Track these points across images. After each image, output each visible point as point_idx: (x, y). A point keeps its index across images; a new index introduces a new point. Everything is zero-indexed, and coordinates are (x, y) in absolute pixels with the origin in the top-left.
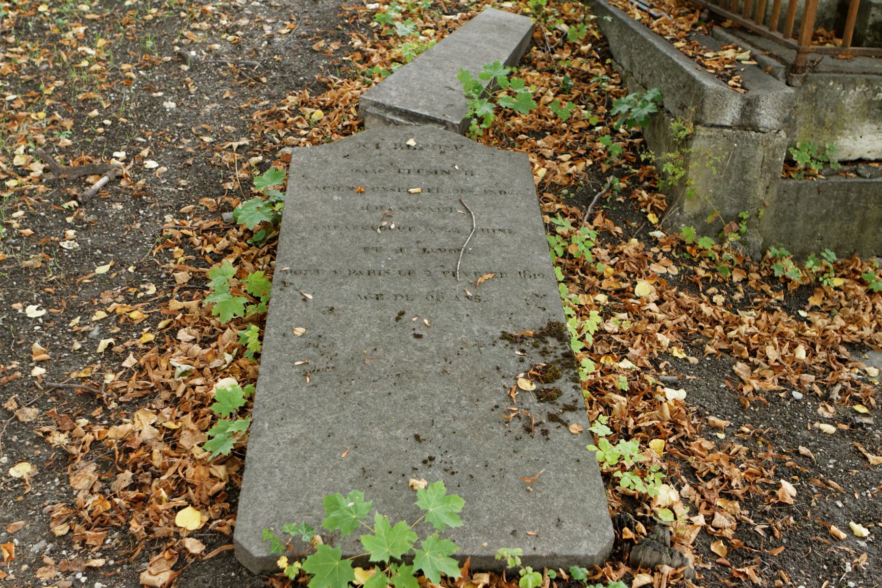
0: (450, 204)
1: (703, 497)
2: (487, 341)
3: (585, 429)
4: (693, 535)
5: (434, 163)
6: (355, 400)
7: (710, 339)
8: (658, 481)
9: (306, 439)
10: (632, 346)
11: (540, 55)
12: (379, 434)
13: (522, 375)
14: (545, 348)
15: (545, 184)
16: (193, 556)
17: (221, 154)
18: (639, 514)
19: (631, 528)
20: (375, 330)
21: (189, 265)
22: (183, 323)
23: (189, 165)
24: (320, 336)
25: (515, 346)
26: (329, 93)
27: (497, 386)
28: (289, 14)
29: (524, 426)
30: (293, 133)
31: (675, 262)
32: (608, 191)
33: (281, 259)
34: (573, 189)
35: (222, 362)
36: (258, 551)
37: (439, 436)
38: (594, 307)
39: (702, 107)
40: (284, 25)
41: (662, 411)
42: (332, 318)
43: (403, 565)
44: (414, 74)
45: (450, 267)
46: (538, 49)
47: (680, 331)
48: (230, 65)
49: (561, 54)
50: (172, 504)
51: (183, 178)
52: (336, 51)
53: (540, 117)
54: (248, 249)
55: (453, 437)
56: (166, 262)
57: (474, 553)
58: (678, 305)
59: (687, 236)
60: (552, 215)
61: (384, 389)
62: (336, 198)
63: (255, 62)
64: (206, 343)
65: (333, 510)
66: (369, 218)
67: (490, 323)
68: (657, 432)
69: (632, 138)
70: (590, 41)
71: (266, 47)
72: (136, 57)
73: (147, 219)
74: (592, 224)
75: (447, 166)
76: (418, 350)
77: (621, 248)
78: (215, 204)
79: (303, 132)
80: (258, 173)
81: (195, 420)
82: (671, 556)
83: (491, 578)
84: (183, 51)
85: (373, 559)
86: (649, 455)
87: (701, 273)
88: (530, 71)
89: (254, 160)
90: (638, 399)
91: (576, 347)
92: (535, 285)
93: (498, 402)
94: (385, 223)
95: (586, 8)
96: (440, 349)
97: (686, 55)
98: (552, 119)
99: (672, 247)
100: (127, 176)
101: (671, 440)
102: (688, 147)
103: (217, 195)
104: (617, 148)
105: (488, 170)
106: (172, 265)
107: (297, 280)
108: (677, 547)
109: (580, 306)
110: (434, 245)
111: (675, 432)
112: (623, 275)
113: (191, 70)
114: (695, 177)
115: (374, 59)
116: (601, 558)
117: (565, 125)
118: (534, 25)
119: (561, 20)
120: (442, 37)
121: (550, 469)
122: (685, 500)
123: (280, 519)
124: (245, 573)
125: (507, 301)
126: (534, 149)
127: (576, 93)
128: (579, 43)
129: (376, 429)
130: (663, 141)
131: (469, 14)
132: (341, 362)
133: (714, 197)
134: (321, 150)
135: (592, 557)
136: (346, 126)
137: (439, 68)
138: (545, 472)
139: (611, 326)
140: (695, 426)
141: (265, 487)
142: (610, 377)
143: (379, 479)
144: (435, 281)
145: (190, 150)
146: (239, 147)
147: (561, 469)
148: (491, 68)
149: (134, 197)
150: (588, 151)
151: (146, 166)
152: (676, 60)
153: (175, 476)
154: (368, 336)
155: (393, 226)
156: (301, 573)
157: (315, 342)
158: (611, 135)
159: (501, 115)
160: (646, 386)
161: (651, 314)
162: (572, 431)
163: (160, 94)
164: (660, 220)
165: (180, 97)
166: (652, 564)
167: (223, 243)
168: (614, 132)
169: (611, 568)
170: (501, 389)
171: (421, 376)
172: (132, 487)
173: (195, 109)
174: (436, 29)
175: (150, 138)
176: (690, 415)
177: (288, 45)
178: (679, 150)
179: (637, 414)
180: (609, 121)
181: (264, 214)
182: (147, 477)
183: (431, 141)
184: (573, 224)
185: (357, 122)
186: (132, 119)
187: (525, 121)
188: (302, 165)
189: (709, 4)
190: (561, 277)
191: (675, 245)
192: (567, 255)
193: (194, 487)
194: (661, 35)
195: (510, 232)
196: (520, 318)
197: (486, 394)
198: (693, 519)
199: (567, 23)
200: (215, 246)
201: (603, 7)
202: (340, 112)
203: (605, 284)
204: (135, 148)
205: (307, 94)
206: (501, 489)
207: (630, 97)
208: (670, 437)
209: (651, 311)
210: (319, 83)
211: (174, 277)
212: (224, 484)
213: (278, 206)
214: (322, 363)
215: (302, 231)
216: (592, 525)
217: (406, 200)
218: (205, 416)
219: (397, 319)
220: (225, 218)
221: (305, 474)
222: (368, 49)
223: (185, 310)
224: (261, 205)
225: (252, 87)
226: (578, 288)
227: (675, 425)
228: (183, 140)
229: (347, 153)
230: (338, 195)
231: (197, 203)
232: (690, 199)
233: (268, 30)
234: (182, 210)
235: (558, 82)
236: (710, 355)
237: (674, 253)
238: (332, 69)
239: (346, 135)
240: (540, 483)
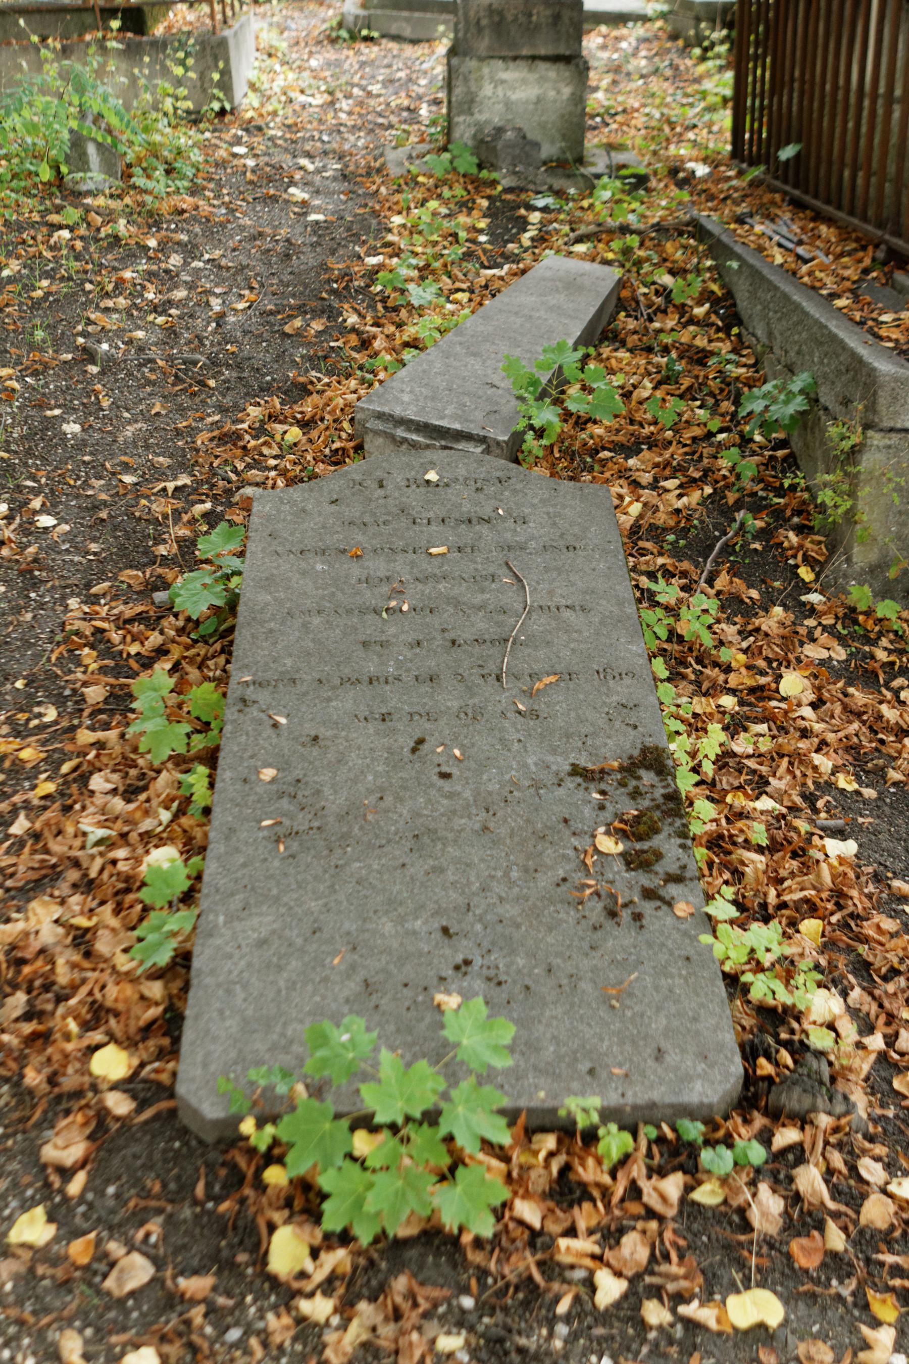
0: (492, 569)
1: (881, 1006)
2: (550, 779)
3: (698, 909)
4: (865, 1065)
5: (466, 507)
6: (352, 875)
7: (895, 759)
8: (811, 985)
9: (280, 937)
10: (774, 775)
11: (632, 324)
12: (388, 927)
13: (602, 829)
14: (637, 787)
15: (640, 527)
16: (117, 1119)
17: (150, 501)
18: (784, 1036)
19: (769, 1058)
20: (380, 769)
21: (105, 674)
22: (98, 764)
23: (103, 520)
24: (298, 781)
25: (592, 786)
26: (309, 400)
27: (564, 847)
28: (247, 279)
29: (605, 908)
30: (257, 464)
31: (842, 640)
32: (736, 534)
33: (240, 664)
34: (683, 532)
35: (156, 822)
36: (211, 1111)
37: (479, 927)
38: (718, 716)
39: (874, 403)
40: (241, 296)
41: (819, 875)
42: (315, 751)
43: (425, 1125)
44: (438, 365)
45: (492, 667)
46: (628, 316)
47: (848, 749)
48: (161, 363)
49: (663, 322)
50: (85, 1042)
51: (94, 540)
52: (319, 333)
53: (632, 422)
54: (193, 646)
55: (499, 928)
56: (70, 672)
57: (533, 1104)
58: (846, 708)
59: (859, 600)
60: (652, 576)
61: (394, 858)
62: (319, 567)
63: (198, 356)
64: (132, 793)
65: (320, 1046)
66: (371, 597)
67: (554, 751)
68: (811, 908)
69: (774, 449)
70: (708, 300)
71: (215, 332)
72: (19, 357)
73: (42, 606)
74: (712, 587)
75: (487, 512)
76: (446, 797)
77: (757, 622)
78: (142, 580)
79: (272, 462)
80: (205, 528)
81: (117, 911)
82: (831, 1100)
83: (559, 1142)
84: (89, 344)
85: (379, 1119)
86: (799, 944)
87: (882, 655)
88: (616, 350)
89: (199, 509)
90: (783, 858)
91: (685, 782)
92: (622, 690)
93: (566, 872)
94: (393, 604)
95: (701, 248)
96: (479, 794)
97: (851, 320)
98: (650, 424)
99: (837, 618)
100: (10, 541)
101: (834, 919)
102: (856, 464)
103: (145, 565)
104: (749, 467)
105: (548, 513)
106: (79, 675)
107: (263, 697)
108: (841, 1086)
109: (695, 715)
110: (466, 635)
111: (839, 907)
112: (761, 663)
113: (103, 373)
114: (867, 509)
115: (377, 344)
116: (723, 1107)
117: (670, 433)
118: (620, 280)
119: (662, 270)
120: (481, 304)
121: (645, 973)
122: (854, 1012)
123: (244, 1060)
124: (194, 1143)
125: (578, 716)
126: (623, 473)
127: (686, 382)
128: (689, 302)
129: (384, 919)
130: (819, 453)
131: (521, 266)
132: (331, 819)
133: (899, 538)
134: (297, 493)
135: (710, 1106)
136: (337, 450)
137: (475, 355)
138: (637, 979)
139: (742, 745)
140: (869, 896)
141: (221, 1012)
142: (740, 824)
143: (389, 996)
144: (471, 690)
145: (103, 496)
146: (177, 489)
147: (662, 971)
148: (553, 351)
149: (22, 573)
150: (706, 472)
151: (39, 524)
152: (835, 330)
153: (90, 999)
154: (370, 778)
155: (405, 608)
156: (276, 1142)
157: (292, 790)
158: (740, 446)
159: (572, 421)
160: (795, 836)
161: (803, 724)
162: (679, 913)
163: (57, 412)
164: (818, 576)
165: (88, 414)
166: (802, 1112)
167: (155, 639)
168: (745, 441)
169: (739, 1120)
170: (571, 853)
171: (450, 836)
172: (28, 1016)
173: (109, 432)
174: (472, 291)
175: (43, 480)
176: (863, 879)
177: (246, 327)
178: (842, 469)
179: (781, 881)
180: (738, 423)
181: (215, 594)
182: (48, 1001)
183: (462, 472)
184: (683, 588)
185: (352, 444)
186: (16, 452)
187: (608, 429)
188: (268, 518)
189: (887, 237)
190: (665, 674)
191: (840, 615)
192: (673, 636)
193: (117, 1014)
194: (813, 288)
195: (583, 609)
196: (598, 742)
197: (548, 861)
198: (867, 1040)
199: (672, 272)
200: (142, 644)
201: (726, 247)
202: (327, 428)
203: (733, 680)
204: (20, 497)
205: (277, 402)
206: (572, 1005)
207: (768, 387)
208: (832, 914)
209: (803, 718)
210: (295, 384)
211: (82, 695)
212: (160, 1009)
213: (235, 580)
214: (302, 822)
215: (270, 620)
216: (710, 1056)
217: (425, 565)
218: (131, 907)
219: (414, 750)
220: (157, 600)
221: (279, 991)
222: (368, 328)
223: (100, 745)
224: (208, 580)
225: (194, 394)
226: (692, 687)
227: (839, 897)
228: (93, 482)
229: (335, 497)
230: (323, 563)
231: (116, 579)
232: (862, 543)
233: (216, 304)
234: (94, 590)
235: (658, 366)
236: (895, 784)
237: (839, 627)
238: (314, 361)
239: (336, 464)
240: (631, 995)
